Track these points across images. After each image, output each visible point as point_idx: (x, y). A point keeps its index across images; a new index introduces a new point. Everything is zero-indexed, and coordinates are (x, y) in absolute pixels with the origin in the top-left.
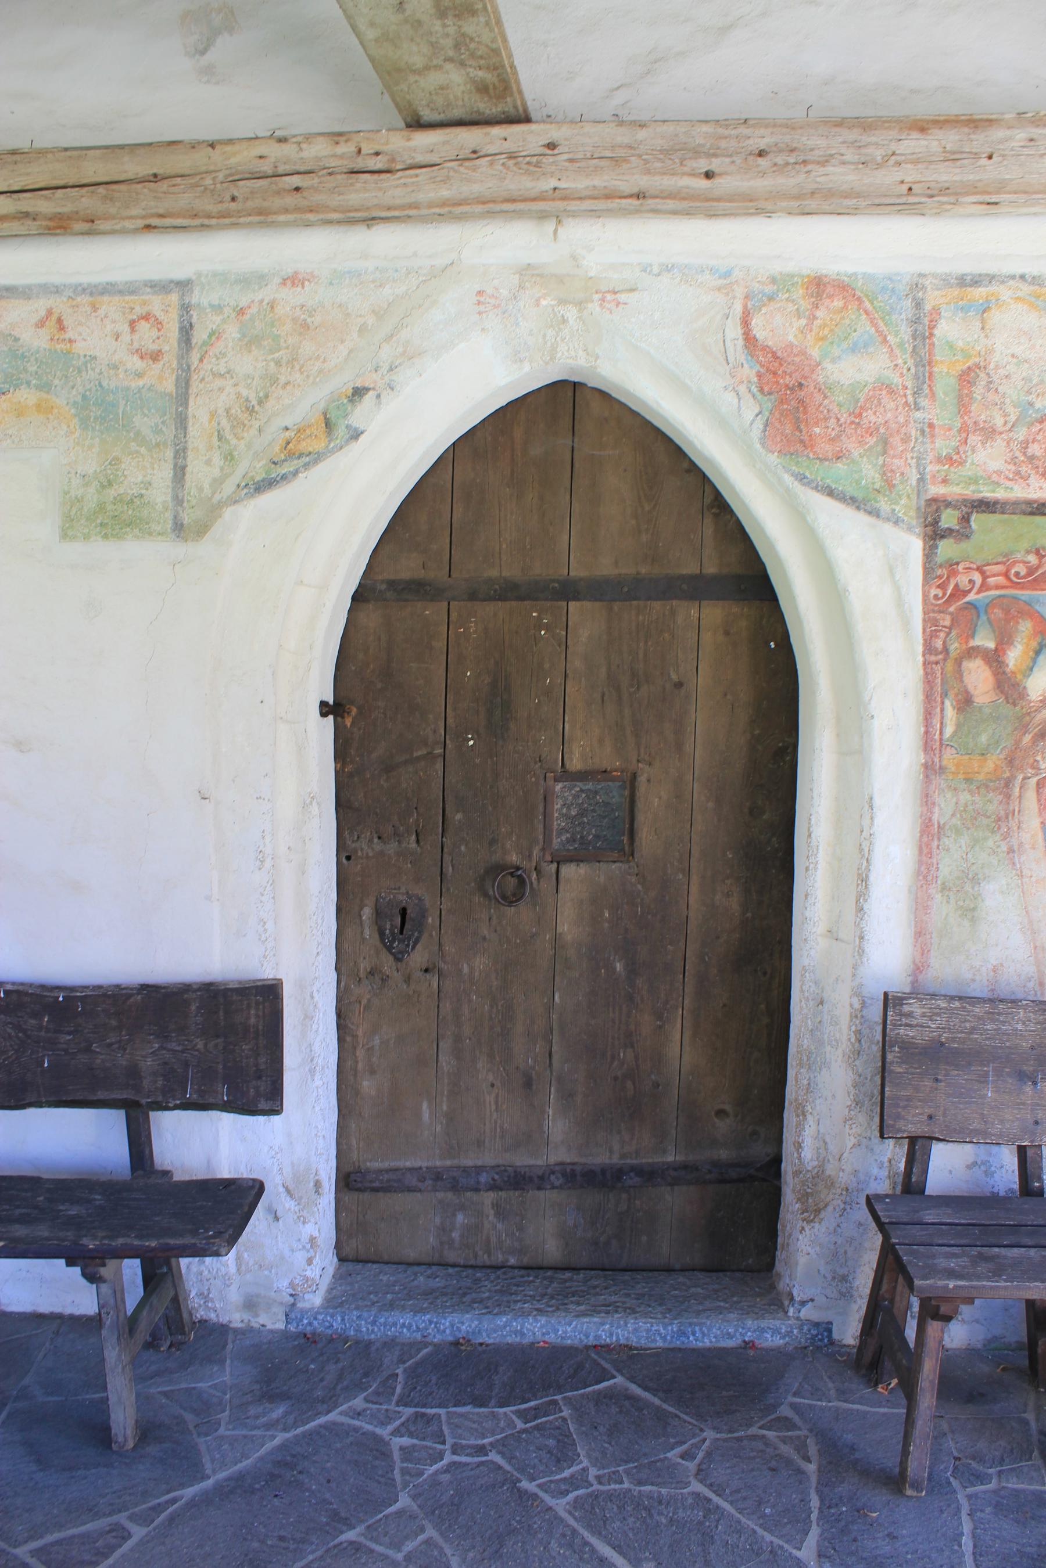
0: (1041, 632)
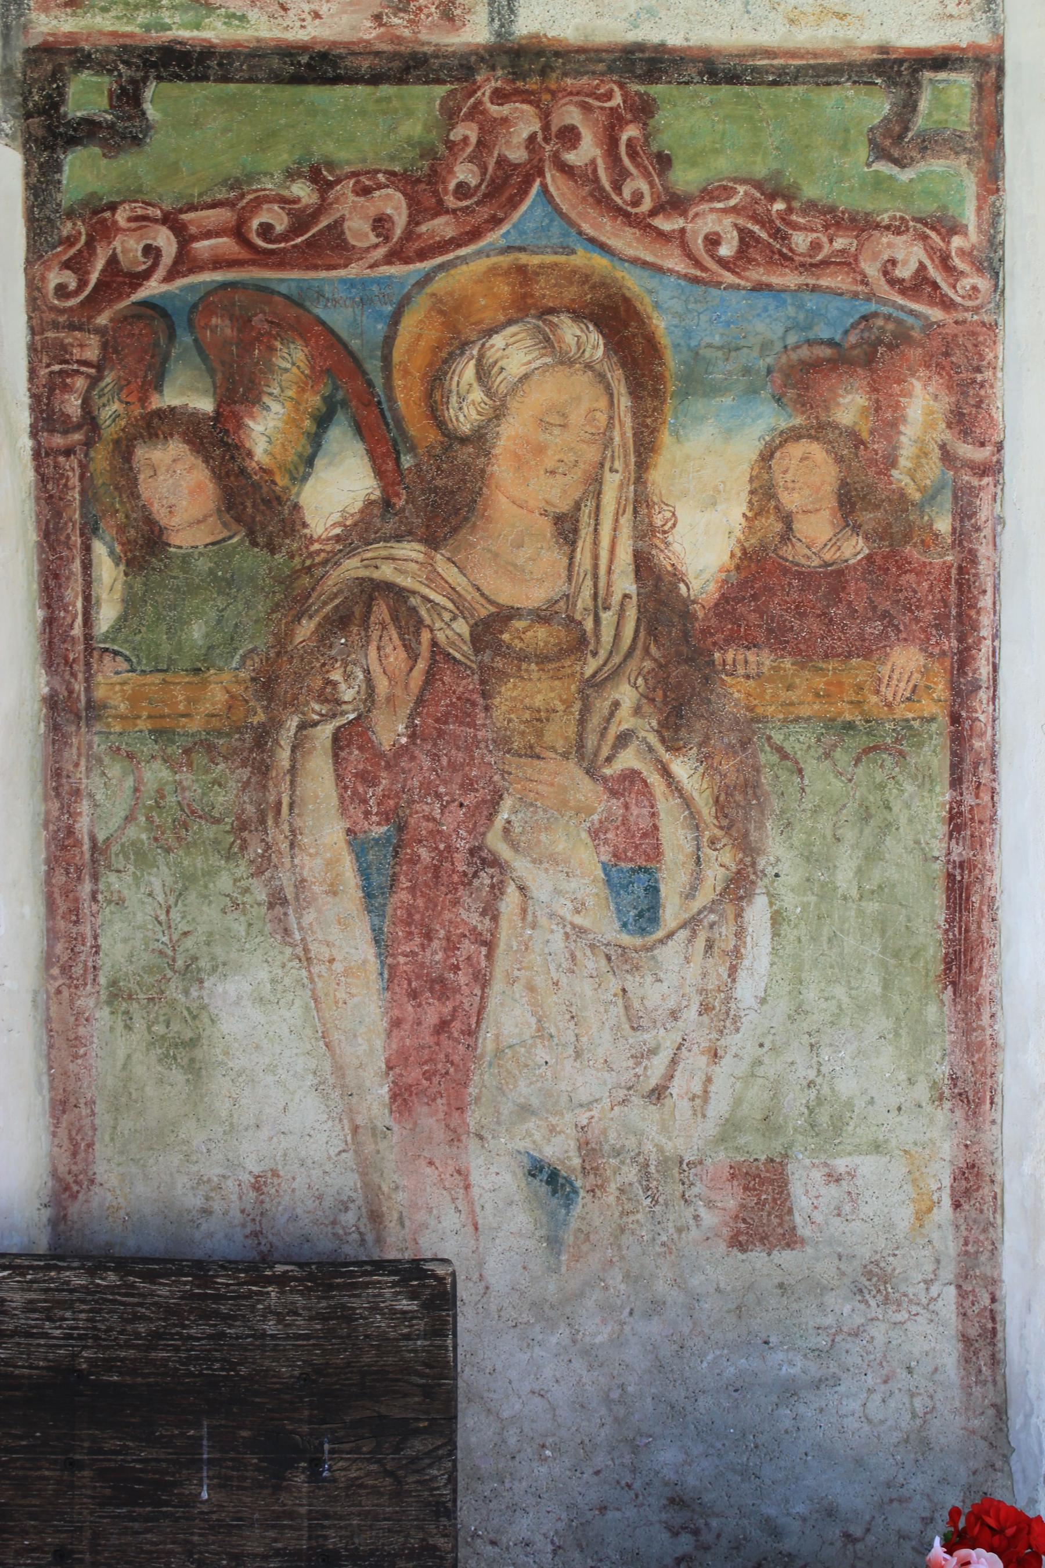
0: (328, 370)
